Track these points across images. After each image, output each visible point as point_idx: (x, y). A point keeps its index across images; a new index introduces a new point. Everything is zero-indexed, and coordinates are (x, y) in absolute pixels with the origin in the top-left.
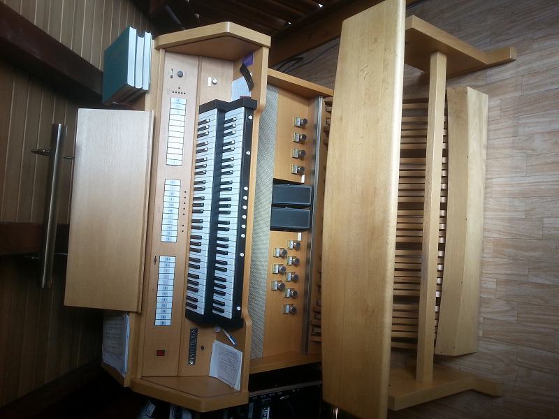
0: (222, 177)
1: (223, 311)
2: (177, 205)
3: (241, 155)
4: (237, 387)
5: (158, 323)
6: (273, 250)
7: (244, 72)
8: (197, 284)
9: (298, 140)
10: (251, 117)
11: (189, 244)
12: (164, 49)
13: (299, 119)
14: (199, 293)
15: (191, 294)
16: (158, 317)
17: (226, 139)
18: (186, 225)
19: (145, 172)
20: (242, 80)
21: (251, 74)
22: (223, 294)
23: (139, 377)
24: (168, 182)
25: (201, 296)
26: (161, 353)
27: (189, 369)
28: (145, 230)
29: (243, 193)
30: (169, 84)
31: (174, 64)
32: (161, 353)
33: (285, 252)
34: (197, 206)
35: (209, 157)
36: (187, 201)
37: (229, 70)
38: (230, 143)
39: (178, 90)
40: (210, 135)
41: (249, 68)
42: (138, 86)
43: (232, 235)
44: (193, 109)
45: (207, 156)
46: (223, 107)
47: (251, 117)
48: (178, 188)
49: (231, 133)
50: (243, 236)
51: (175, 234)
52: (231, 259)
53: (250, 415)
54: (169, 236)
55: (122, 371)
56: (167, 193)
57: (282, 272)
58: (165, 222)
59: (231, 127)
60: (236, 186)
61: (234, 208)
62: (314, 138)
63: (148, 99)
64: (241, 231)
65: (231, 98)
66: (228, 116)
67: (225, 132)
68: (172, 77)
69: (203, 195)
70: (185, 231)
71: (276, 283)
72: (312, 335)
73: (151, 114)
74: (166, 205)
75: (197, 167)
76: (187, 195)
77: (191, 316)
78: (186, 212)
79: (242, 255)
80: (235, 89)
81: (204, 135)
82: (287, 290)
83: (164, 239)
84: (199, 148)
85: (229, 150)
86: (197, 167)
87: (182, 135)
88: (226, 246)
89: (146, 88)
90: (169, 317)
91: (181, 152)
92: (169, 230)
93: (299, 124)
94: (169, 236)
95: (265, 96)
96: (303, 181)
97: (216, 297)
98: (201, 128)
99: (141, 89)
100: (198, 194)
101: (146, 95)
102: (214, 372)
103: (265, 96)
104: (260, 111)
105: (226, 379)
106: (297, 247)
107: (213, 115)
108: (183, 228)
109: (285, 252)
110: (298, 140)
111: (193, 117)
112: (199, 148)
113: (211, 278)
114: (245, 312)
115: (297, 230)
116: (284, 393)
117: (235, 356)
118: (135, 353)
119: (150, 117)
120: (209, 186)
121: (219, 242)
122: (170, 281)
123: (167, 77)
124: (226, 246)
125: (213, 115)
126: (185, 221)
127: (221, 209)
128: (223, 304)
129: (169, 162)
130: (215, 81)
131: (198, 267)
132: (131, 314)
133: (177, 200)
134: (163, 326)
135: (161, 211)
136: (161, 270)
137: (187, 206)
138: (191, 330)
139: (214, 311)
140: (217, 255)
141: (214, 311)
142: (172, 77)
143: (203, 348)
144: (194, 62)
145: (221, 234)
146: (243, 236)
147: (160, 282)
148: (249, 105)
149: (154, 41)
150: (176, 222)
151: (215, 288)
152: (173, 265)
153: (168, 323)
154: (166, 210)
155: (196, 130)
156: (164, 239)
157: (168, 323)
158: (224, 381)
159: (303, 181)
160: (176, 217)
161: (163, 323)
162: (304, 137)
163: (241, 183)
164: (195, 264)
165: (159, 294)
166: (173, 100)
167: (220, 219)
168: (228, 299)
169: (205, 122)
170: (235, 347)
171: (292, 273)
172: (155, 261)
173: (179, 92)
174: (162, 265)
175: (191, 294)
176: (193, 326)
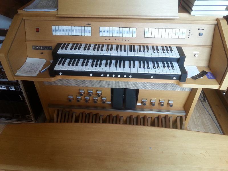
1: (59, 65)
2: (121, 35)
3: (151, 73)
4: (18, 74)
5: (54, 27)
7: (203, 73)
8: (98, 50)
9: (143, 101)
10: (175, 78)
11: (102, 43)
12: (217, 24)
13: (172, 102)
14: (106, 52)
15: (92, 46)
16: (57, 27)
17: (160, 64)
18: (109, 41)
19: (150, 15)
20: (198, 72)
21: (202, 78)
22: (92, 65)
23: (24, 18)
24: (135, 29)
25: (68, 51)
26: (38, 30)
27: (29, 46)
29: (128, 75)
30: (195, 29)
31: (207, 30)
32: (38, 30)
33: (99, 96)
34: (121, 47)
35: (150, 53)
36: (124, 42)
37: (203, 64)
38: (158, 66)
39: (191, 33)
40: (153, 53)
41: (205, 76)
42: (194, 8)
43: (103, 69)
44: (179, 43)
45: (150, 52)
46: (181, 61)
47: (175, 78)
48: (131, 36)
49: (164, 66)
50: (102, 75)
51: (104, 35)
52: (89, 68)
53: (2, 80)
54: (103, 31)
55: (26, 9)
56: (128, 29)
57: (89, 94)
59: (168, 66)
60: (132, 70)
61: (118, 70)
62: (162, 110)
63: (185, 15)
64: (105, 74)
65: (186, 65)
66: (176, 64)
67: (165, 63)
68: (199, 29)
70: (106, 41)
71: (92, 92)
72: (58, 110)
74: (121, 29)
75: (144, 46)
76: (127, 42)
77: (58, 46)
78: (117, 41)
79: (91, 75)
80: (192, 70)
81: (163, 50)
82: (97, 97)
83: (101, 28)
84: (165, 48)
85: (154, 66)
86: (144, 46)
87: (163, 36)
88: (120, 67)
89: (192, 13)
90: (57, 34)
91: (153, 36)
92: (107, 32)
93: (170, 102)
94: (103, 31)
95: (187, 86)
96: (138, 104)
98: (167, 49)
99: (192, 10)
100: (128, 48)
101: (188, 14)
102: (29, 60)
103: (187, 86)
104: (178, 84)
105: (24, 67)
106: (103, 102)
107: (176, 55)
108: (108, 39)
109: (99, 96)
110: (160, 102)
111: (174, 43)
112: (165, 48)
113: (101, 58)
114: (58, 77)
115: (112, 100)
116: (23, 97)
117: (35, 72)
118: (37, 15)
120: (133, 54)
121: (122, 62)
122: (128, 34)
124: (120, 67)
126: (111, 41)
127: (142, 62)
128: (100, 66)
130: (196, 56)
131: (94, 50)
132: (57, 11)
133: (124, 36)
134: (52, 30)
135: (118, 26)
136: (83, 28)
137: (121, 41)
138: (51, 47)
139: (60, 59)
140: (115, 61)
141: (60, 59)
142: (199, 29)
143: (42, 53)
144: (209, 42)
145: (127, 63)
146: (102, 75)
147: (76, 28)
148: (182, 78)
149: (222, 17)
150: (111, 35)
151: (73, 60)
152: (86, 34)
153: (54, 33)
154: (118, 29)
155: (166, 45)
156: (101, 28)
157: (54, 33)
158: (23, 66)
159: (138, 104)
160: (114, 35)
161: (54, 30)
162: (162, 105)
163: (134, 73)
165: (70, 27)
166: (185, 31)
167: (136, 62)
168: (66, 67)
169: (171, 50)
170: (40, 72)
171: (97, 100)
172: (88, 24)
174: (86, 28)
175: (92, 46)
176: (53, 48)
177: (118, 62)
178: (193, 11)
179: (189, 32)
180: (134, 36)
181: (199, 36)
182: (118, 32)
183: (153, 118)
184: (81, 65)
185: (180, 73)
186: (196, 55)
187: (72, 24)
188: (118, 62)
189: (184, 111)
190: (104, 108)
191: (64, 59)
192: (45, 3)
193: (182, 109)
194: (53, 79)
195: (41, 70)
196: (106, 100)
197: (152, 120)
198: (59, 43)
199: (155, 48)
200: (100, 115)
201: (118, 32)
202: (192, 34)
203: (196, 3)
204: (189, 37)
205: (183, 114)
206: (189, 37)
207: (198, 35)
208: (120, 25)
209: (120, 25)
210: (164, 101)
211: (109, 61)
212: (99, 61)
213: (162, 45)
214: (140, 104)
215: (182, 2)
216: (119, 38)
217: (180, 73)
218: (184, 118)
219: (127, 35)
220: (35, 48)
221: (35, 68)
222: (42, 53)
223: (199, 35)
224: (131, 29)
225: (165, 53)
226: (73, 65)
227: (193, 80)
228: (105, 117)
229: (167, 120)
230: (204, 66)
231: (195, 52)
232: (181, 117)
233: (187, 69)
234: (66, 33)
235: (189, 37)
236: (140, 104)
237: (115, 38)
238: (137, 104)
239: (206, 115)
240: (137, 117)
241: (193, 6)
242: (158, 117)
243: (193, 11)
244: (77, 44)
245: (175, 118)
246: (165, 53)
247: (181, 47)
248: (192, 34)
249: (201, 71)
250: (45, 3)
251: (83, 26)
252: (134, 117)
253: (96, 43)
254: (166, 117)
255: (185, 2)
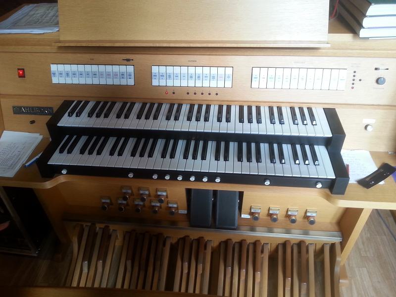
0: (289, 146)
2: (199, 84)
6: (314, 209)
8: (147, 118)
13: (314, 215)
20: (371, 168)
21: (382, 183)
24: (229, 71)
28: (192, 45)
36: (209, 97)
39: (357, 79)
41: (390, 179)
42: (366, 22)
44: (330, 100)
46: (334, 144)
48: (221, 85)
50: (155, 177)
56: (214, 70)
58: (177, 69)
59: (305, 157)
63: (346, 38)
65: (347, 154)
66: (321, 151)
68: (376, 69)
69: (181, 118)
73: (324, 42)
77: (66, 107)
86: (301, 109)
89: (363, 33)
90: (163, 83)
93: (308, 214)
96: (243, 216)
97: (160, 143)
98: (303, 113)
99: (361, 26)
107: (323, 130)
111: (318, 99)
118: (19, 42)
119: (319, 42)
120: (224, 128)
123: (377, 63)
125: (323, 130)
129: (256, 71)
131: (168, 118)
133: (206, 84)
139: (67, 136)
140: (185, 142)
142: (376, 69)
143: (33, 122)
153: (155, 83)
155: (301, 105)
159: (243, 216)
161: (54, 74)
162: (294, 221)
164: (174, 112)
167: (210, 143)
170: (24, 166)
173: (354, 80)
174: (123, 68)
177: (193, 143)
178: (364, 28)
179: (354, 76)
180: (228, 84)
181: (376, 84)
182: (191, 77)
183: (274, 246)
184: (108, 153)
185: (332, 175)
186: (369, 128)
187: (93, 59)
188: (193, 143)
189: (339, 233)
190: (174, 223)
191: (75, 137)
192: (38, 15)
193: (336, 228)
194: (49, 185)
195: (26, 163)
196: (177, 208)
197: (273, 249)
198: (66, 101)
199: (276, 114)
200: (167, 237)
201: (191, 77)
202: (360, 80)
203: (373, 9)
204: (353, 88)
205: (337, 240)
206: (353, 86)
207: (375, 79)
208: (196, 61)
209: (196, 61)
210: (298, 214)
211: (172, 142)
212: (151, 141)
213: (292, 105)
214: (248, 217)
215: (337, 5)
216: (195, 91)
217: (332, 175)
218: (338, 248)
219: (213, 84)
220: (18, 110)
221: (16, 156)
222: (33, 122)
223: (377, 81)
224: (221, 70)
225: (297, 124)
226: (90, 153)
227: (361, 189)
228: (177, 240)
229: (304, 250)
230: (387, 151)
231: (366, 121)
232: (333, 246)
233: (346, 162)
234: (80, 79)
235: (353, 88)
236: (248, 217)
237: (187, 91)
238: (241, 216)
239: (385, 234)
240: (241, 243)
241: (365, 16)
242: (285, 244)
243: (364, 28)
244: (106, 103)
245: (319, 247)
246: (297, 124)
247: (335, 109)
248: (360, 80)
249: (379, 165)
250: (38, 15)
251: (116, 63)
252: (236, 242)
253: (146, 101)
254: (300, 244)
255: (343, 6)
